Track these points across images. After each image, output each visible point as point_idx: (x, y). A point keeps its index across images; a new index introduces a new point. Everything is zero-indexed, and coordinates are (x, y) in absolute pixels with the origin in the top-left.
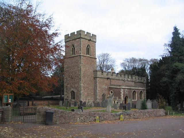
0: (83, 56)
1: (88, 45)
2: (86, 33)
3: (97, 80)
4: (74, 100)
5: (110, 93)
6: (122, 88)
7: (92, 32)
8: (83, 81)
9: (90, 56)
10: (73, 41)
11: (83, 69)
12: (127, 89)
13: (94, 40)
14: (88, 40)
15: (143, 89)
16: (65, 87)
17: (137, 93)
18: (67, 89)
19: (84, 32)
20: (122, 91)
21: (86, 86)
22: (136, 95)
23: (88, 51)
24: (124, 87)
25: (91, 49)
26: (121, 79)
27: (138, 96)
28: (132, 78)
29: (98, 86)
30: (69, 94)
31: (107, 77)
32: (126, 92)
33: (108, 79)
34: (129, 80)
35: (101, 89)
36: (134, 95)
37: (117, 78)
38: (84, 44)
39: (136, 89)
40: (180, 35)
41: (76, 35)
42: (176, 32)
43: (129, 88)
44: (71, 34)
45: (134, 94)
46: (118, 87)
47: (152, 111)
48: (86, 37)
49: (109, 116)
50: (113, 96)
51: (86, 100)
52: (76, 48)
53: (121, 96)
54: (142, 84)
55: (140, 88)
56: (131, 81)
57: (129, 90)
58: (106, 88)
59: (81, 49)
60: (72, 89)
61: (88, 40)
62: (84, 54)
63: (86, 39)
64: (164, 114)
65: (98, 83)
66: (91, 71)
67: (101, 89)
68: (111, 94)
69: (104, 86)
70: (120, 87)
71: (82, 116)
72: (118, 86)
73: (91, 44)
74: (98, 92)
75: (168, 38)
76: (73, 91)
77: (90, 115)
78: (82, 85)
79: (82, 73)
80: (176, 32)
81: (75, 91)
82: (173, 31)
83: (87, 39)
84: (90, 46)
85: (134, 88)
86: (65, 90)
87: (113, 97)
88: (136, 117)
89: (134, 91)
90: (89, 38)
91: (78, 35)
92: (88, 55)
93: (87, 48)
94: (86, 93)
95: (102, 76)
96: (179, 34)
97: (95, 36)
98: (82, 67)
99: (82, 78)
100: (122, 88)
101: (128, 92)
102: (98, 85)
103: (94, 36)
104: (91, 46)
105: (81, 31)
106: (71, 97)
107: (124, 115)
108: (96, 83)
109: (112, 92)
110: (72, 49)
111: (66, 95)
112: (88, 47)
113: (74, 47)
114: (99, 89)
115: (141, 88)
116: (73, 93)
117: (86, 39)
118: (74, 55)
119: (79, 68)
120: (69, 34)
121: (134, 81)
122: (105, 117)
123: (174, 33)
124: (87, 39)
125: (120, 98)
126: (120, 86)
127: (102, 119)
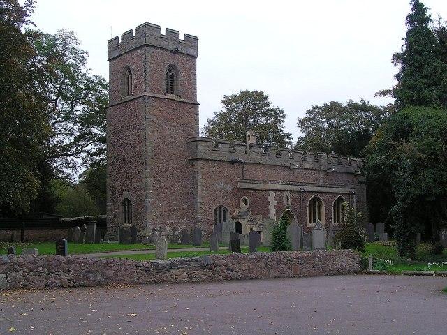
0: (153, 97)
1: (171, 67)
2: (182, 38)
3: (199, 168)
4: (130, 225)
5: (242, 204)
6: (273, 190)
7: (183, 30)
8: (152, 169)
9: (178, 99)
10: (128, 56)
11: (153, 136)
12: (291, 191)
13: (191, 52)
14: (171, 51)
15: (347, 191)
16: (109, 187)
17: (324, 205)
18: (113, 195)
19: (158, 28)
20: (272, 197)
21: (163, 184)
22: (323, 209)
23: (171, 83)
24: (279, 187)
25: (181, 79)
26: (279, 163)
27: (328, 213)
28: (317, 160)
29: (199, 184)
30: (118, 208)
31: (230, 157)
32: (285, 199)
33: (233, 162)
34: (307, 166)
35: (209, 192)
36: (338, 211)
37: (266, 160)
38: (157, 64)
39: (321, 193)
40: (430, 26)
41: (135, 38)
42: (418, 16)
43: (298, 188)
44: (123, 35)
45: (314, 207)
46: (262, 187)
47: (303, 257)
48: (163, 44)
49: (125, 270)
50: (247, 212)
51: (165, 224)
52: (134, 77)
53: (269, 212)
54: (286, 171)
55: (334, 190)
56: (315, 170)
57: (296, 195)
58: (227, 191)
59: (149, 78)
60: (126, 194)
61: (171, 51)
62: (158, 92)
63: (162, 49)
64: (357, 267)
65: (199, 177)
66: (180, 140)
67: (209, 192)
68: (244, 207)
69: (221, 185)
70: (266, 187)
71: (16, 267)
72: (260, 182)
73: (179, 62)
74: (199, 200)
75: (395, 37)
76: (127, 200)
77: (48, 267)
78: (150, 180)
79: (150, 147)
80: (418, 16)
81: (133, 200)
82: (408, 10)
83: (166, 50)
84: (176, 69)
85: (315, 189)
86: (109, 195)
87: (249, 216)
88: (237, 275)
89: (315, 199)
90: (172, 47)
91: (139, 38)
92: (169, 96)
93: (167, 74)
94: (163, 206)
95: (216, 156)
96: (428, 19)
97: (195, 39)
98: (149, 130)
99: (149, 162)
100: (273, 190)
101: (293, 200)
102: (200, 181)
103: (192, 41)
104: (179, 68)
105: (146, 25)
106: (122, 215)
107: (189, 268)
108: (194, 175)
109: (245, 202)
110: (126, 80)
111: (111, 210)
112: (170, 71)
113: (130, 72)
114: (205, 193)
115: (341, 190)
116: (127, 202)
117: (162, 49)
118: (129, 97)
119: (143, 133)
120: (118, 38)
121: (322, 168)
122: (110, 273)
123: (411, 19)
124: (166, 50)
125: (266, 217)
126: (266, 182)
127: (96, 277)
